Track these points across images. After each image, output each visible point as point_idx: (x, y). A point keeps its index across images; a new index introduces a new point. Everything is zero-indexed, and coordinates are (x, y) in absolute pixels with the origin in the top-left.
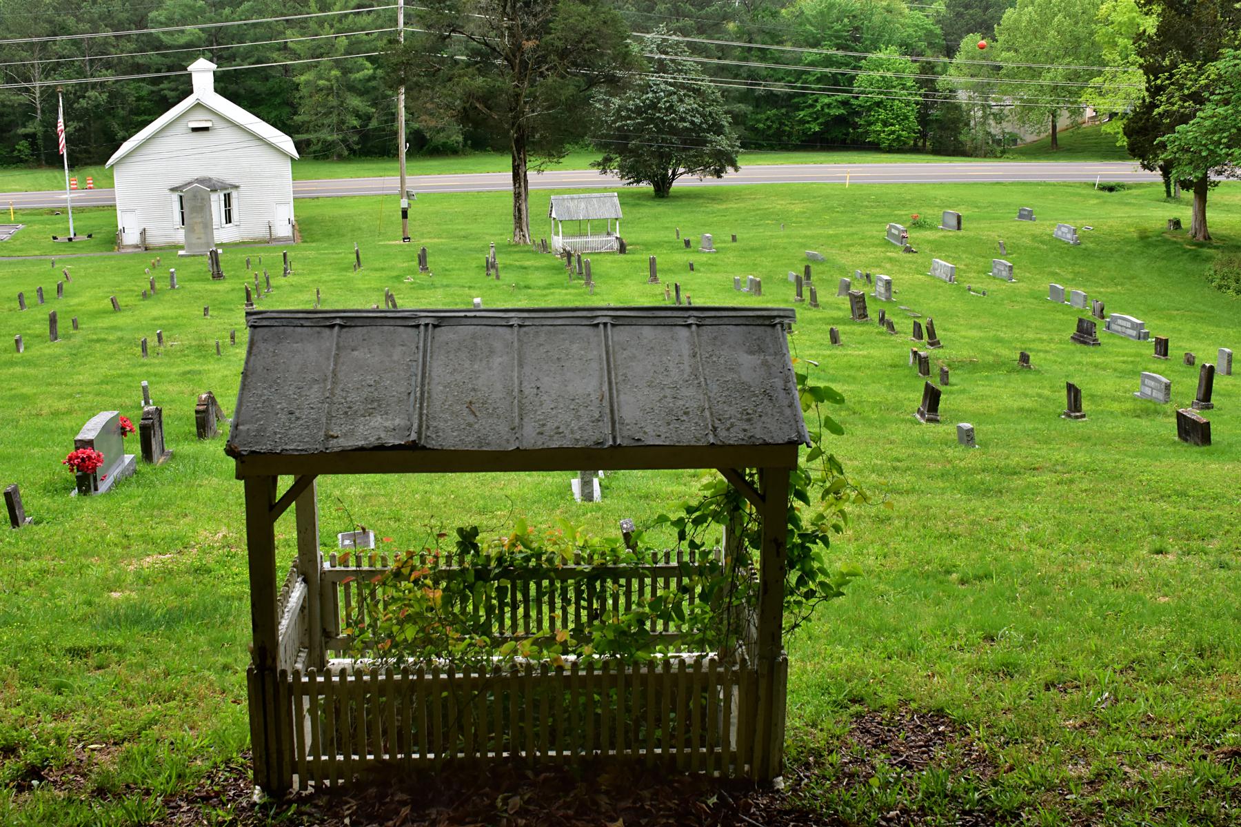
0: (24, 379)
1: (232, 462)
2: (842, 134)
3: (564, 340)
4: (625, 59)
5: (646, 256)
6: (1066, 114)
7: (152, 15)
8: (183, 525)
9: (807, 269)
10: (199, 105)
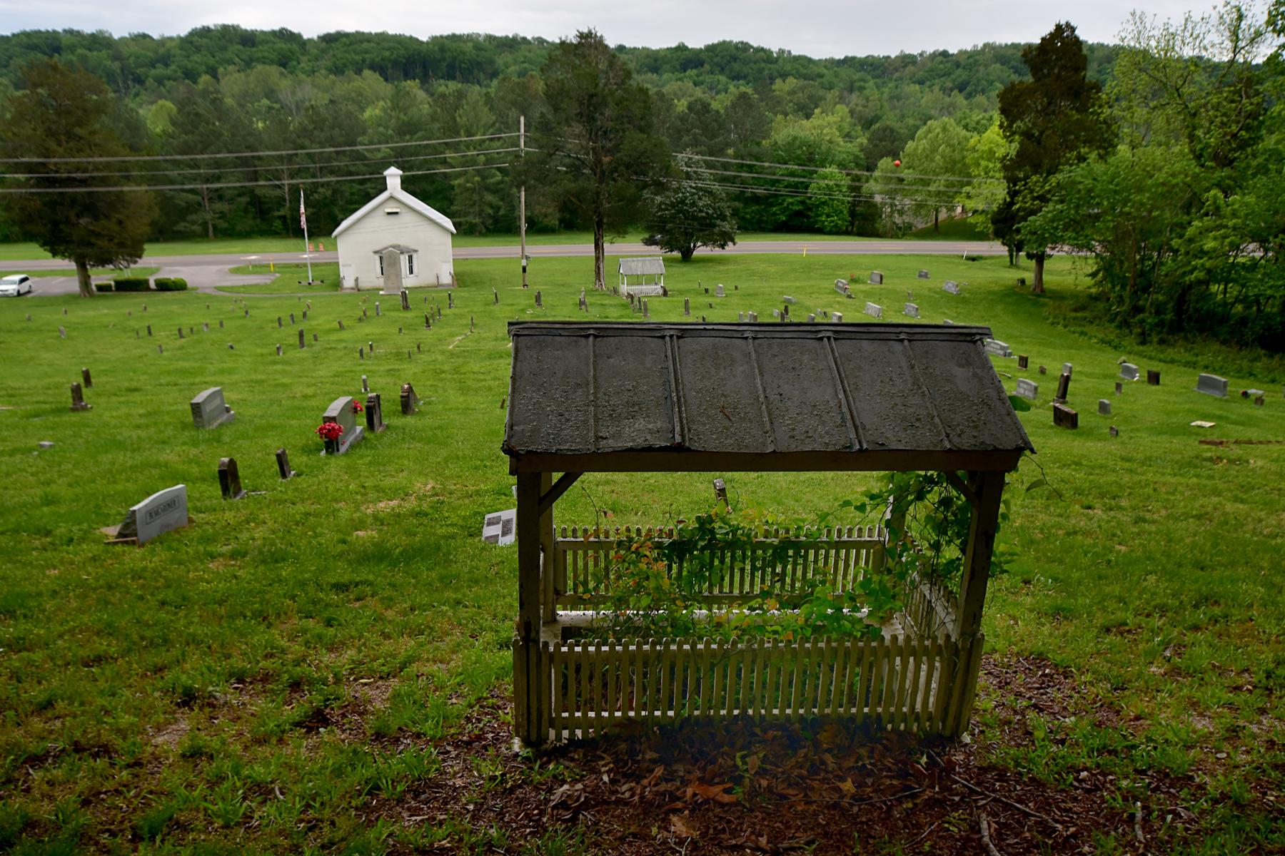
0: (283, 372)
1: (507, 458)
2: (801, 222)
3: (795, 351)
4: (667, 170)
5: (683, 299)
6: (944, 210)
7: (360, 139)
8: (402, 478)
9: (786, 308)
10: (392, 197)
